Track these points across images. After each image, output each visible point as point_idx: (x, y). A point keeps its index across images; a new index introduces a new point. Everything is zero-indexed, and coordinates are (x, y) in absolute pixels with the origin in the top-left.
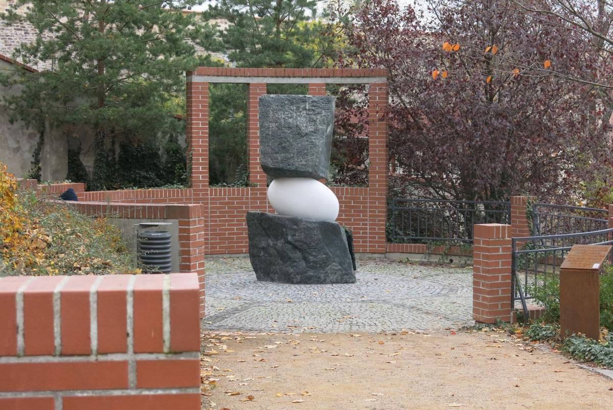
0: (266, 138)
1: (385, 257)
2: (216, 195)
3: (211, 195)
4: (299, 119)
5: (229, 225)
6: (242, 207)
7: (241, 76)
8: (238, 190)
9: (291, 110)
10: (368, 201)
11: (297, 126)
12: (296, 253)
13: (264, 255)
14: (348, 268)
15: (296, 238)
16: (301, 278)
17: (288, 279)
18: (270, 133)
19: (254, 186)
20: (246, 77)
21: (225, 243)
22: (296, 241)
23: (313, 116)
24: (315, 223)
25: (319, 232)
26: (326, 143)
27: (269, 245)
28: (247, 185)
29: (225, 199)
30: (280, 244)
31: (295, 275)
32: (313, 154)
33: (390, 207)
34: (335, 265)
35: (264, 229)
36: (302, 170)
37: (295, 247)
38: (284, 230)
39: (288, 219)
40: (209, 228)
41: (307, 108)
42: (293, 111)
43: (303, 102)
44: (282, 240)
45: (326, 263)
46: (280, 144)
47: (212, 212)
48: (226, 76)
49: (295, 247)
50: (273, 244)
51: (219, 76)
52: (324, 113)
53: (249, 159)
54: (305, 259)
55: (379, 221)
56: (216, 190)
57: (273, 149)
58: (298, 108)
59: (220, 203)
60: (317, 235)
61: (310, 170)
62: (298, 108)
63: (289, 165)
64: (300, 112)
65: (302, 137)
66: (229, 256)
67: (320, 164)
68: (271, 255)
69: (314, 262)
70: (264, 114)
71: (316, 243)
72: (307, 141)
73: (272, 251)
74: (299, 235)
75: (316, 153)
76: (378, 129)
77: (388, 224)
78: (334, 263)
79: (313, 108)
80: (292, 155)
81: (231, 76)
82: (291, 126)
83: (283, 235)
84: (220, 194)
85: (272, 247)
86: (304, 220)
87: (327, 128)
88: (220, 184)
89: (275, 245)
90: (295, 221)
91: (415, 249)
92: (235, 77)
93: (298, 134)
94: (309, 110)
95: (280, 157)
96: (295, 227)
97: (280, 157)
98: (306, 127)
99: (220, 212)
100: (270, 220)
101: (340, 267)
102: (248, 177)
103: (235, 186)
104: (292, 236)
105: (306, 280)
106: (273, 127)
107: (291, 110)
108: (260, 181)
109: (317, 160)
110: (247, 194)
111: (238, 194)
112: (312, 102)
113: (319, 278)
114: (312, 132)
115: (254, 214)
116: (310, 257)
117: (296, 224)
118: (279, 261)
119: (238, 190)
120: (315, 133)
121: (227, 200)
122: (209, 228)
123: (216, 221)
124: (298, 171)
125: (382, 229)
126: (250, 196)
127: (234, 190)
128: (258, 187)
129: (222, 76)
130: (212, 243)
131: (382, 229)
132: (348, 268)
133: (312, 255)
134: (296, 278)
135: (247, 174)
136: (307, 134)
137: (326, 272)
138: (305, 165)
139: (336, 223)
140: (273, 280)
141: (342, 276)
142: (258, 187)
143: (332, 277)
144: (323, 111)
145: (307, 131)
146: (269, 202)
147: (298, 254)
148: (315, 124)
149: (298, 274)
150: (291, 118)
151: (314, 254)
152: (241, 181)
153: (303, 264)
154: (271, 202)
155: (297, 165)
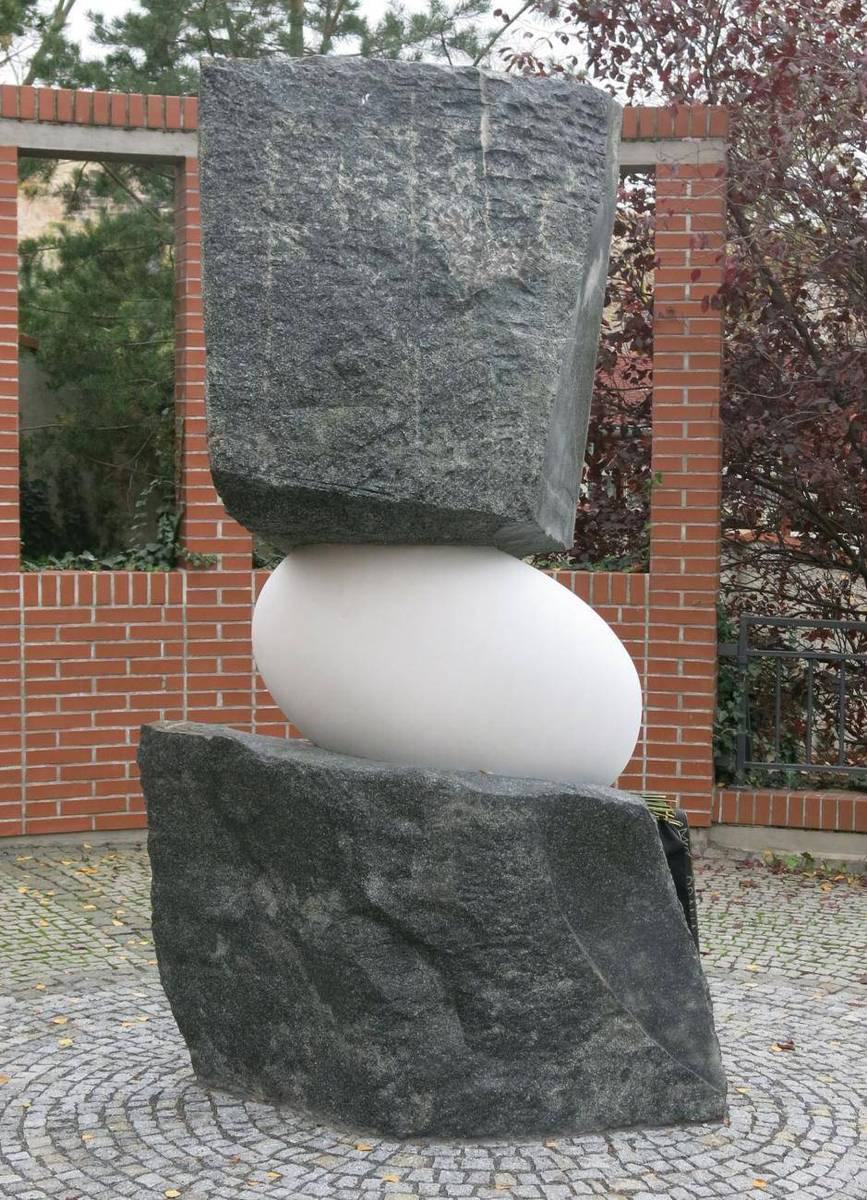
0: (244, 311)
1: (710, 843)
2: (49, 599)
3: (31, 600)
4: (436, 201)
5: (100, 720)
6: (155, 650)
7: (154, 129)
8: (140, 583)
9: (391, 146)
10: (647, 625)
11: (425, 245)
12: (409, 969)
13: (230, 959)
14: (691, 1044)
15: (414, 886)
16: (437, 1106)
17: (361, 1106)
18: (268, 282)
19: (202, 567)
20: (172, 131)
21: (86, 790)
22: (415, 904)
23: (516, 194)
24: (517, 803)
25: (539, 854)
26: (578, 349)
27: (256, 911)
28: (175, 562)
29: (86, 616)
30: (319, 912)
31: (401, 1092)
32: (515, 415)
33: (730, 649)
34: (623, 1033)
35: (230, 823)
36: (453, 505)
37: (405, 939)
38: (344, 841)
39: (367, 783)
40: (23, 734)
41: (484, 140)
42: (402, 154)
43: (460, 104)
44: (335, 897)
45: (575, 1021)
46: (327, 346)
47: (32, 670)
48: (92, 124)
49: (405, 939)
50: (282, 911)
51: (63, 123)
52: (573, 180)
53: (183, 457)
54: (464, 1005)
55: (689, 702)
56: (49, 582)
57: (279, 380)
58: (432, 138)
59: (66, 634)
60: (530, 867)
61: (499, 506)
62: (432, 138)
63: (377, 474)
64: (445, 163)
65: (454, 308)
66: (101, 839)
67: (546, 468)
68: (267, 966)
69: (513, 1019)
70: (231, 162)
71: (524, 911)
72: (483, 334)
73: (277, 945)
74: (429, 875)
75: (534, 404)
76: (687, 345)
77: (722, 715)
78: (618, 1021)
79: (518, 145)
80: (394, 416)
81: (110, 125)
82: (394, 242)
83: (340, 873)
84: (67, 599)
85: (273, 924)
86: (457, 782)
87: (587, 269)
88: (69, 557)
89: (289, 916)
90: (407, 795)
91: (829, 816)
92: (129, 129)
93: (433, 294)
94: (491, 153)
95: (321, 425)
96: (405, 826)
97: (321, 425)
98: (477, 252)
99: (67, 670)
100: (267, 780)
101: (649, 1042)
102: (179, 530)
103: (130, 566)
104: (391, 876)
105: (468, 1120)
106: (281, 248)
107: (391, 146)
108: (224, 546)
109: (538, 449)
110: (176, 598)
111: (140, 597)
112: (514, 108)
113: (536, 1103)
114: (510, 281)
115: (179, 744)
116: (491, 994)
117: (416, 815)
118: (316, 1002)
119: (140, 583)
120: (525, 290)
121: (93, 622)
122: (23, 734)
123: (50, 704)
124: (429, 510)
125: (700, 735)
126: (184, 605)
127: (122, 583)
128: (220, 569)
129: (73, 123)
130: (33, 793)
131: (700, 735)
132: (691, 1044)
133: (499, 984)
134: (411, 1109)
135: (175, 520)
136: (479, 295)
137: (576, 1073)
138: (469, 476)
139: (624, 797)
140: (277, 1097)
141: (660, 1086)
142: (220, 569)
143: (608, 1097)
144: (571, 170)
145: (481, 279)
146: (260, 680)
147: (424, 977)
148: (528, 241)
149: (420, 1086)
150: (387, 196)
151: (510, 974)
152: (151, 547)
153: (448, 1030)
154: (267, 680)
155: (423, 473)
